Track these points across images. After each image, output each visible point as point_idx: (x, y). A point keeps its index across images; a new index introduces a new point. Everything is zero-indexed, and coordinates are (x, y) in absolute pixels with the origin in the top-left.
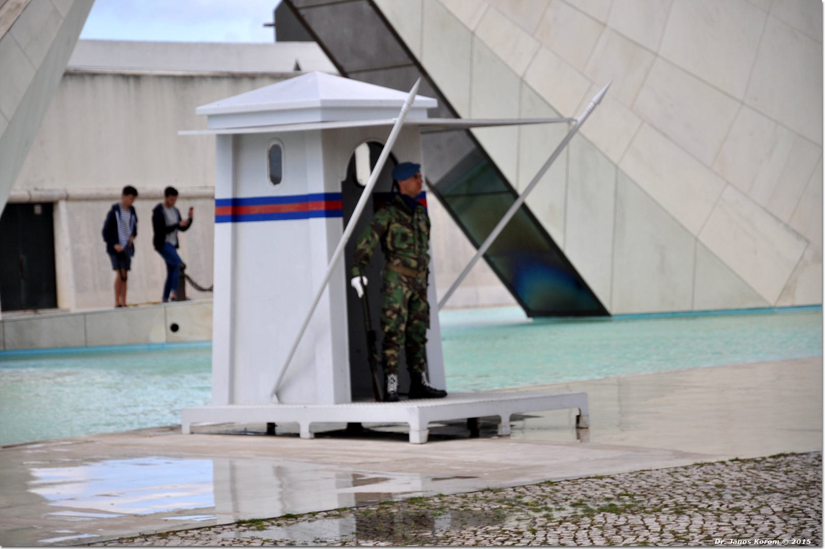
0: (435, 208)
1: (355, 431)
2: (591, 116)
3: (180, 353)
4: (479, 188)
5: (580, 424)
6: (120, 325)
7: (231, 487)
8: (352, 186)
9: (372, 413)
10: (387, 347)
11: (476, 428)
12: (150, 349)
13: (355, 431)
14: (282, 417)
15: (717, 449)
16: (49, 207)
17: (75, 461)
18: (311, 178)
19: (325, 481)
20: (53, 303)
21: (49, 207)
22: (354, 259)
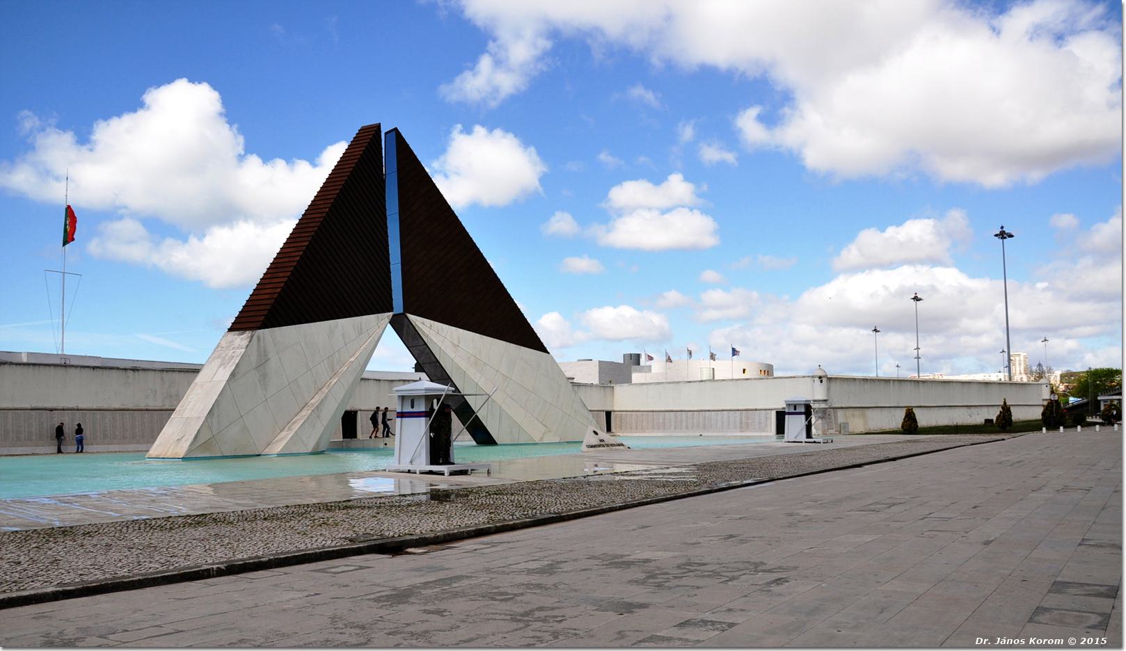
0: (454, 416)
1: (431, 472)
2: (858, 462)
3: (387, 451)
4: (466, 412)
5: (489, 472)
6: (372, 443)
7: (399, 486)
8: (432, 409)
9: (397, 452)
10: (439, 450)
11: (463, 473)
12: (380, 449)
13: (431, 472)
14: (412, 468)
15: (522, 479)
16: (356, 412)
17: (360, 477)
18: (421, 407)
19: (422, 486)
20: (355, 436)
21: (356, 412)
22: (432, 428)
